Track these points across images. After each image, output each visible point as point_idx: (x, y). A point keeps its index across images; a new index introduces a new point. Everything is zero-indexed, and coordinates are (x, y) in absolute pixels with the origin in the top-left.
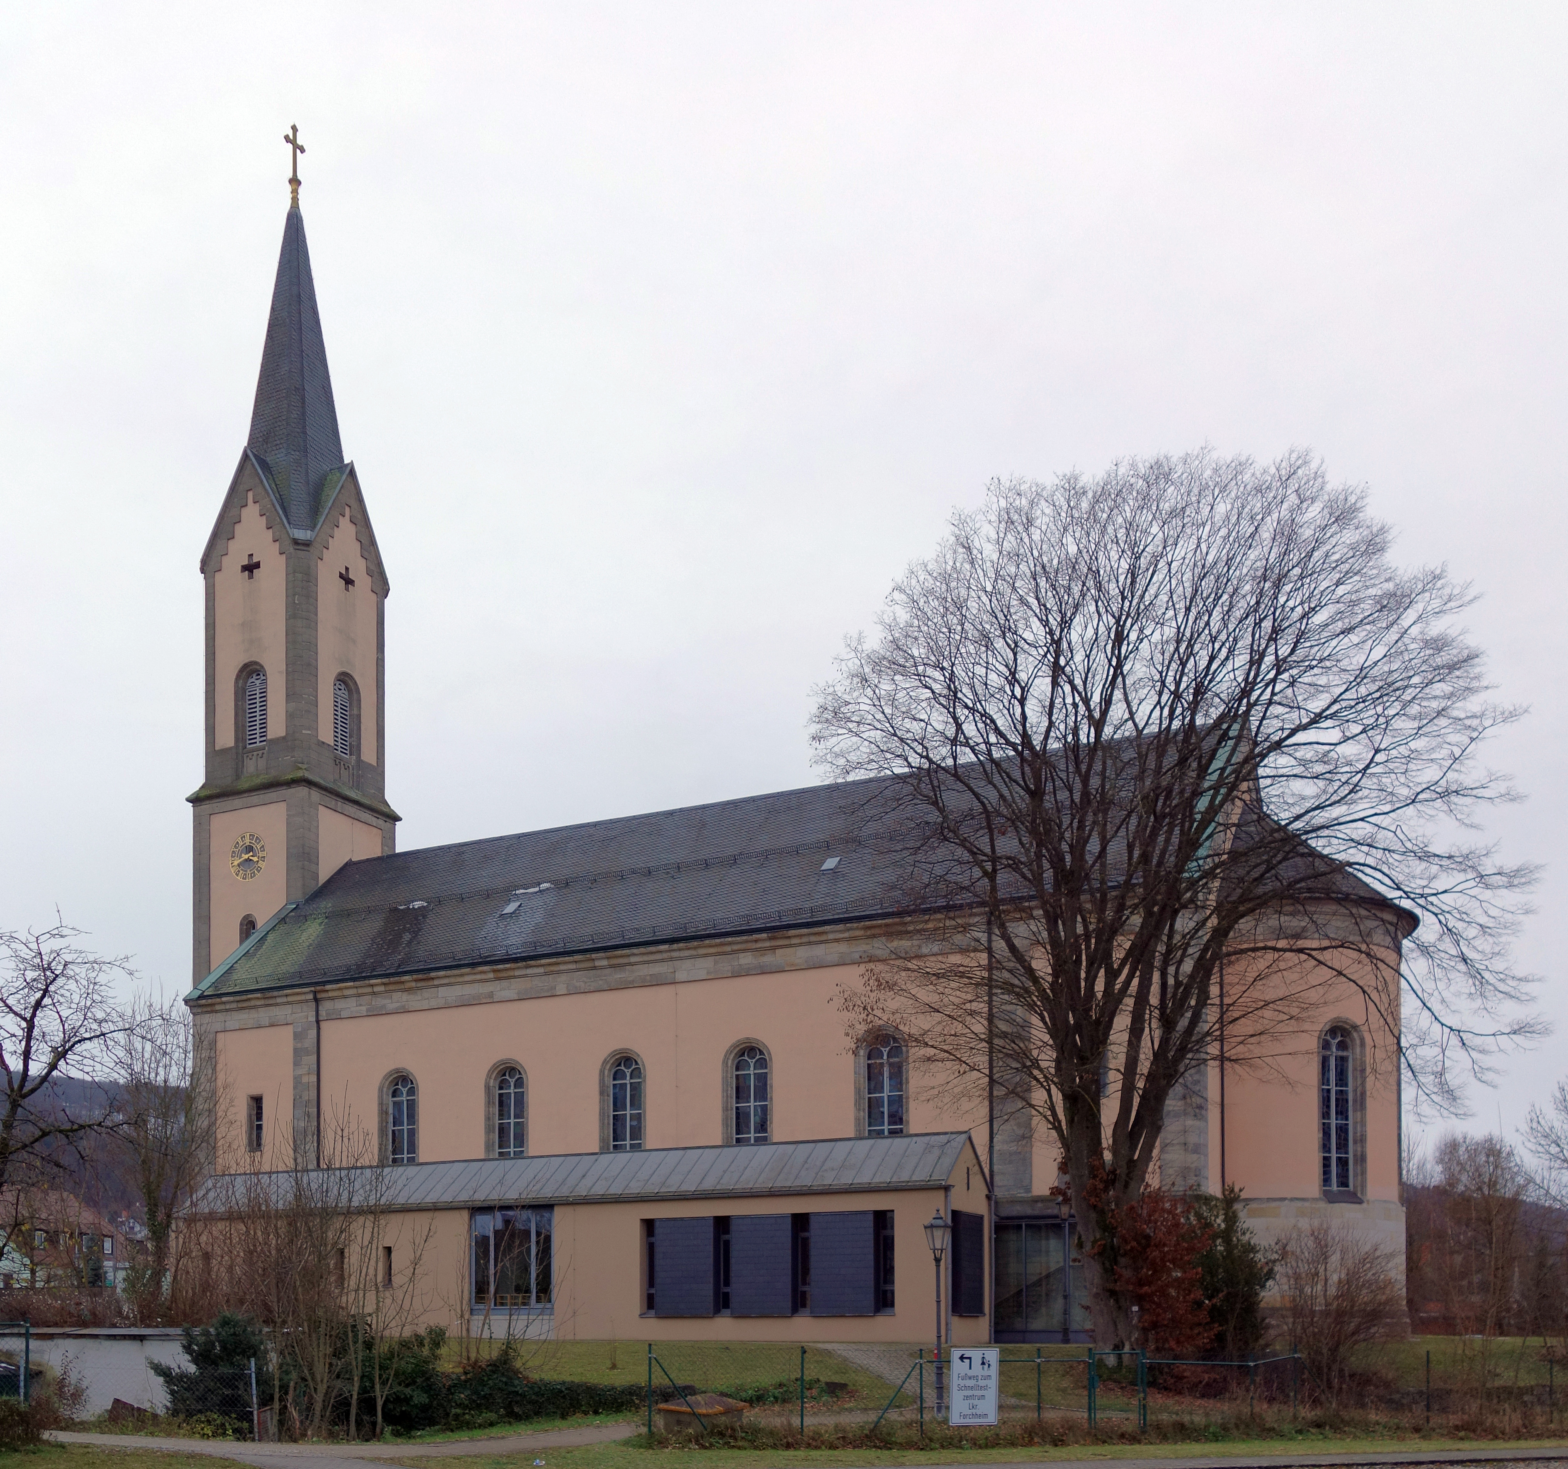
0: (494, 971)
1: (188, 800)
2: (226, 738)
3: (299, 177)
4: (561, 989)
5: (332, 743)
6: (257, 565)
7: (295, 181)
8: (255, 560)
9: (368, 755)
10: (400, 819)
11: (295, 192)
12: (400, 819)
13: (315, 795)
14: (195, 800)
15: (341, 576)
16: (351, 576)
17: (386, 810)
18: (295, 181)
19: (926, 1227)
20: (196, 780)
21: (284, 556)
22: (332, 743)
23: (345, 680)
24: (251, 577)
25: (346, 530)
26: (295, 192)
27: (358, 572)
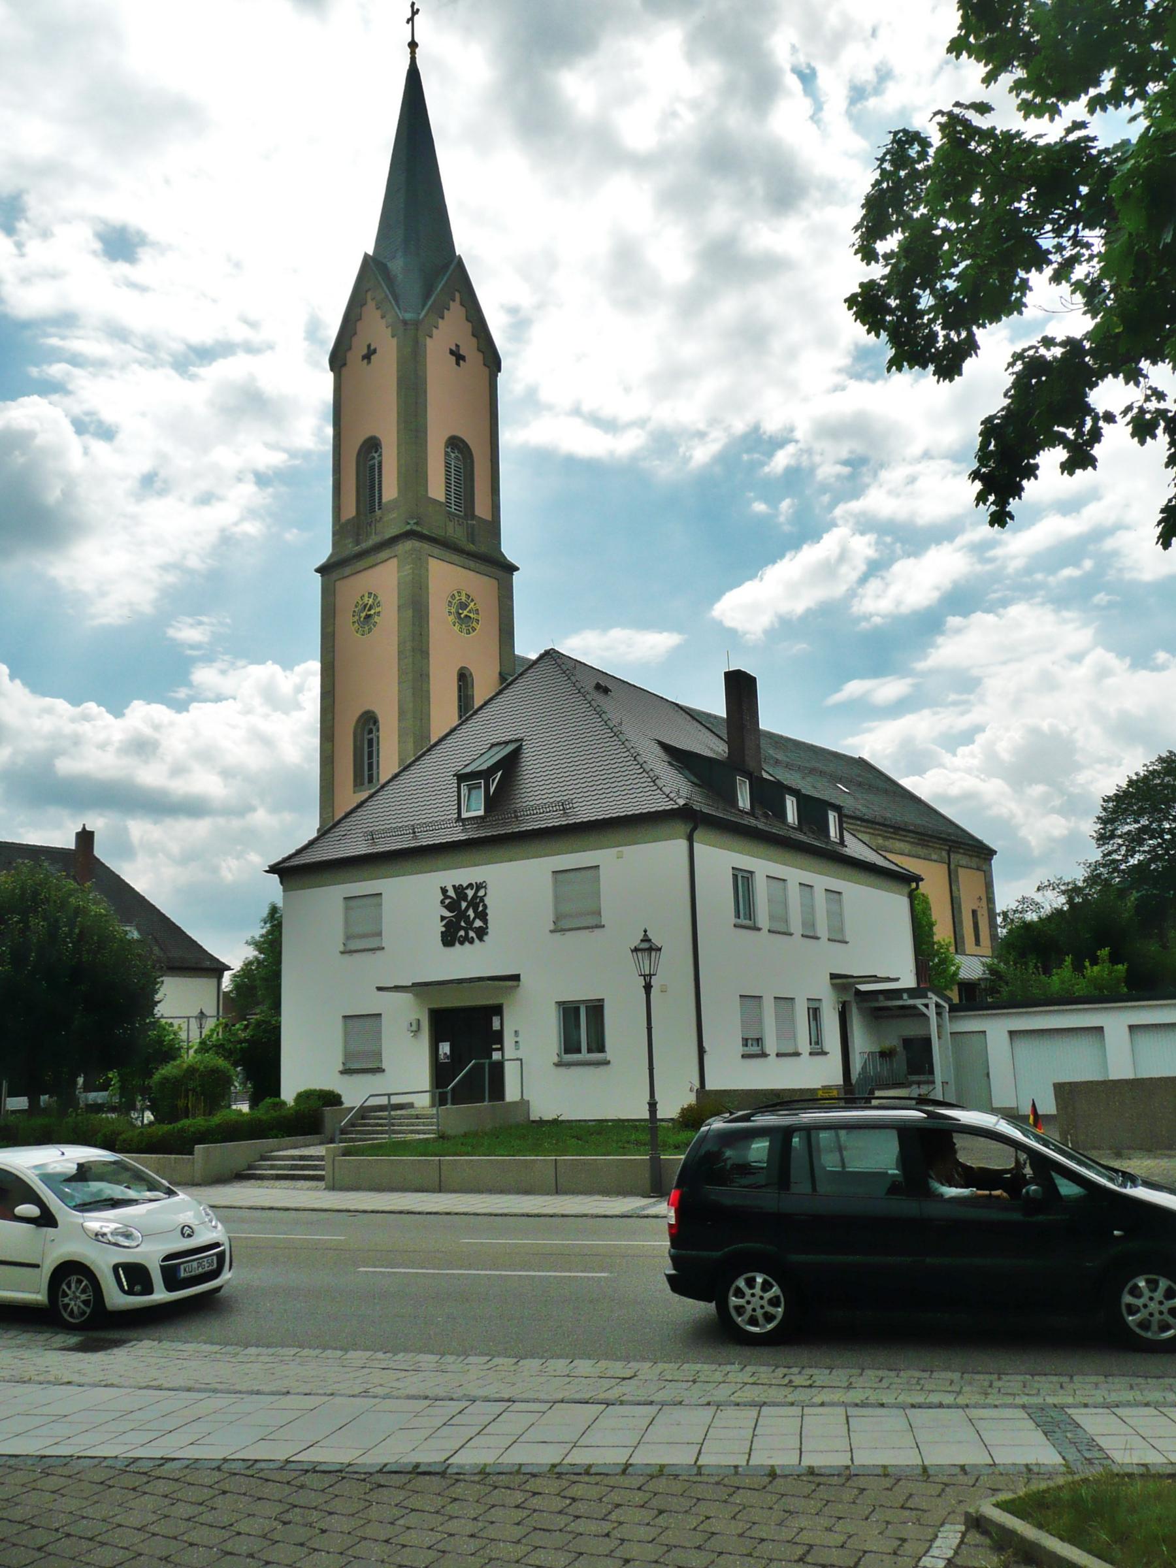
0: (919, 839)
1: (317, 571)
2: (350, 511)
3: (416, 40)
4: (974, 865)
5: (442, 499)
6: (375, 351)
7: (413, 45)
8: (372, 348)
9: (482, 510)
10: (517, 569)
11: (413, 53)
12: (517, 569)
13: (426, 547)
14: (322, 570)
15: (452, 352)
16: (461, 352)
17: (910, 818)
18: (413, 45)
19: (632, 951)
20: (324, 551)
21: (395, 339)
22: (442, 499)
23: (456, 444)
24: (369, 362)
25: (456, 312)
26: (413, 53)
27: (469, 348)
